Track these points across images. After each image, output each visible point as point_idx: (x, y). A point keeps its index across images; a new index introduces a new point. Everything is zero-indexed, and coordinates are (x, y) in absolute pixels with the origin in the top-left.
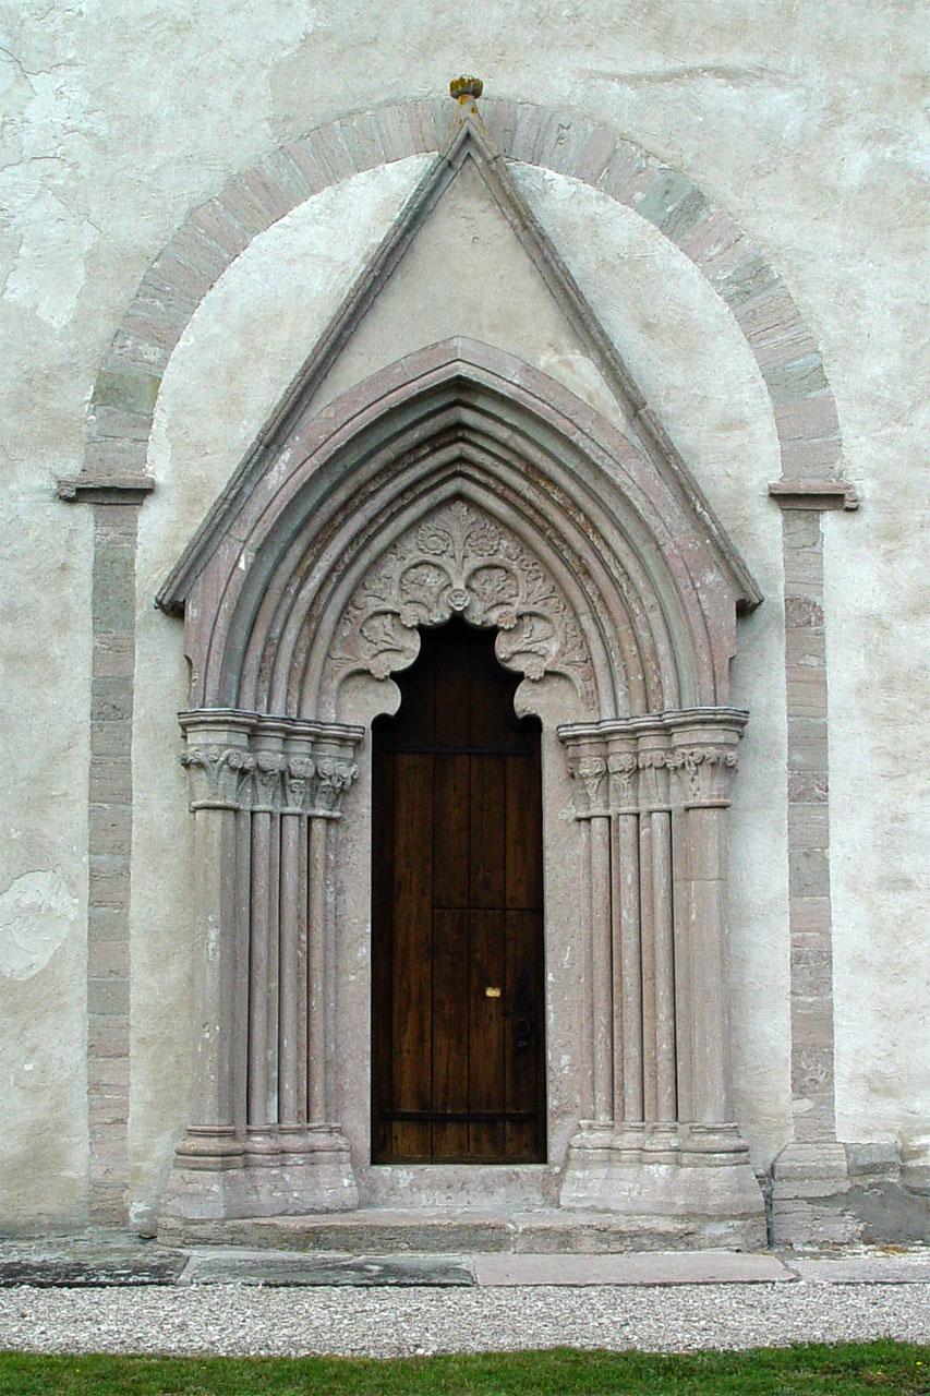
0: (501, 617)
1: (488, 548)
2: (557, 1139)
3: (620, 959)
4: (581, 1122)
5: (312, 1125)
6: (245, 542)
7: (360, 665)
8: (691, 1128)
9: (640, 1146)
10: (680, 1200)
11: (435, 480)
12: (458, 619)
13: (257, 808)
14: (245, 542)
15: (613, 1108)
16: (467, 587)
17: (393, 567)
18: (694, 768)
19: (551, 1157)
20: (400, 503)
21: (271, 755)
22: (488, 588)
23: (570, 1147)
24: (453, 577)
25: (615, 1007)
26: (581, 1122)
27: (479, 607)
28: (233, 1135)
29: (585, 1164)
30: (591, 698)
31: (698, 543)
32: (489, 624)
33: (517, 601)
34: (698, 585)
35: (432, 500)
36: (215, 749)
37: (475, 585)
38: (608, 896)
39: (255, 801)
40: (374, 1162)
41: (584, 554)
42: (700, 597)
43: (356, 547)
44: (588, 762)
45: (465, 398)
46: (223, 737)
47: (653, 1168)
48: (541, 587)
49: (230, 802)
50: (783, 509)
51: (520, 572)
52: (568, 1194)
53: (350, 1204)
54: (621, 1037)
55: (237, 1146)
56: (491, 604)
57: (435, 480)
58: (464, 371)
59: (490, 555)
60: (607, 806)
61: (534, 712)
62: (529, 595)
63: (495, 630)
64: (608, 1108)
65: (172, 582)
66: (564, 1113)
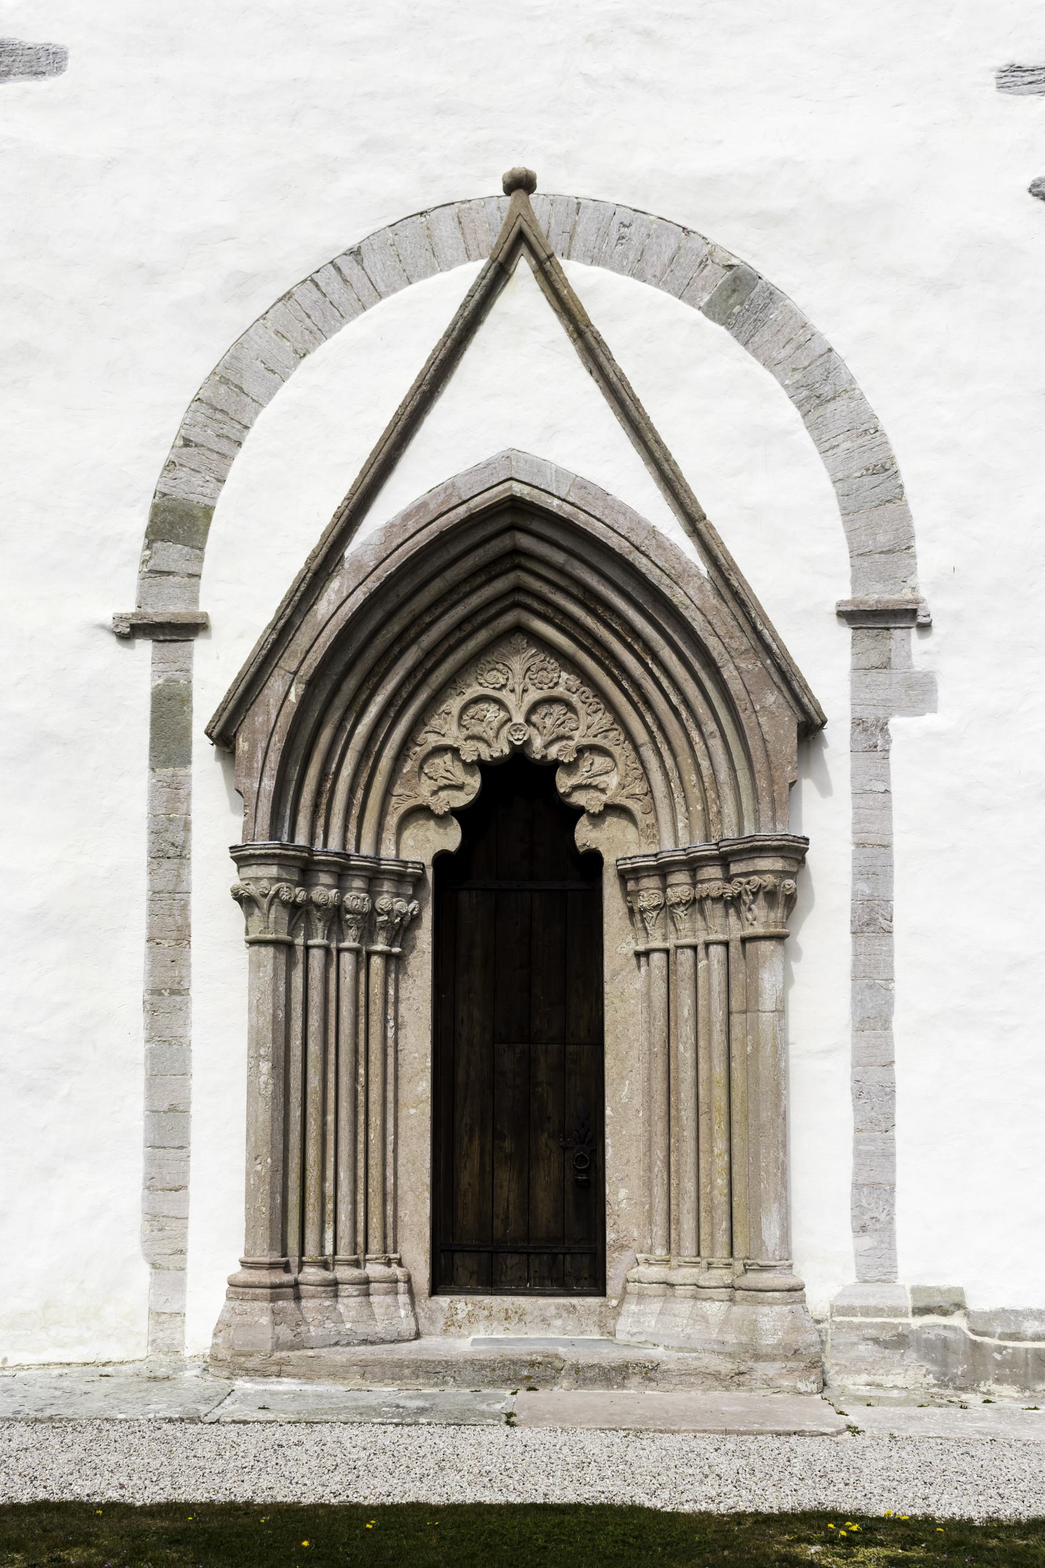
0: (560, 750)
1: (547, 681)
2: (617, 1268)
3: (678, 1093)
4: (638, 1256)
5: (368, 1257)
6: (295, 673)
7: (419, 801)
8: (745, 1266)
9: (694, 1281)
10: (731, 1338)
11: (492, 611)
12: (519, 754)
13: (311, 942)
14: (295, 673)
15: (669, 1243)
16: (528, 721)
17: (454, 704)
18: (751, 897)
19: (609, 1291)
20: (459, 635)
21: (324, 892)
22: (549, 722)
23: (628, 1281)
24: (513, 712)
25: (672, 1141)
26: (638, 1256)
27: (538, 742)
28: (286, 1268)
29: (641, 1296)
30: (652, 833)
31: (759, 664)
32: (549, 758)
33: (577, 734)
34: (758, 708)
35: (491, 632)
36: (265, 883)
37: (534, 718)
38: (666, 1029)
39: (308, 936)
40: (434, 1291)
41: (643, 682)
42: (761, 720)
43: (414, 682)
44: (645, 895)
45: (520, 521)
46: (273, 871)
47: (707, 1305)
48: (603, 719)
49: (283, 936)
50: (853, 628)
51: (580, 704)
52: (624, 1326)
53: (406, 1334)
54: (677, 1171)
55: (287, 1278)
56: (551, 738)
57: (492, 611)
58: (518, 489)
59: (549, 688)
60: (665, 938)
61: (594, 846)
62: (589, 728)
63: (556, 764)
64: (664, 1242)
65: (220, 716)
66: (622, 1247)
